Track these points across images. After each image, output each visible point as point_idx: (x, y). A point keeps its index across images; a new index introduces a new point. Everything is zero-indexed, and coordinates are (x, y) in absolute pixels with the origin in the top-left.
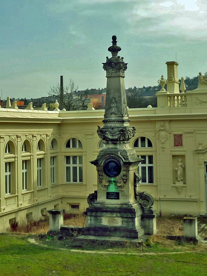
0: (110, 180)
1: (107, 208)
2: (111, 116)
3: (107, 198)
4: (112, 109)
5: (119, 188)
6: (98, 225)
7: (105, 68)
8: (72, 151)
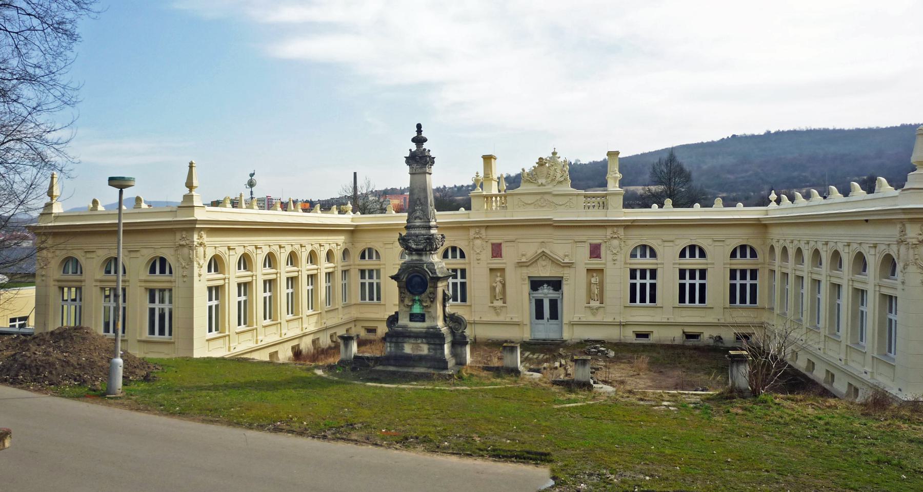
0: (414, 298)
1: (411, 332)
3: (411, 320)
8: (368, 264)
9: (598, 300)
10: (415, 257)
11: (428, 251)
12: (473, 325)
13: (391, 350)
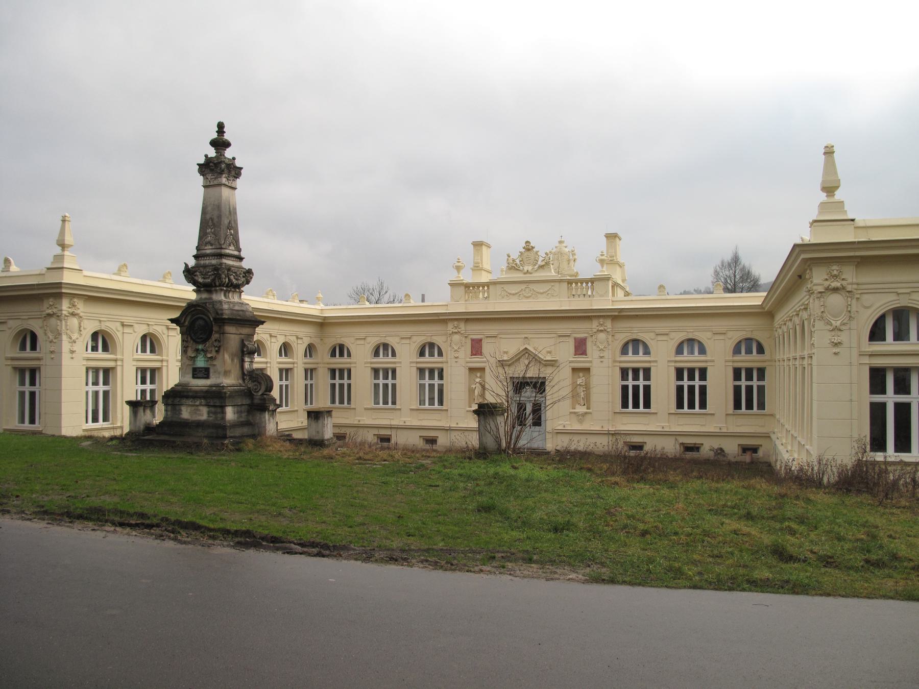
2: (206, 248)
3: (194, 377)
5: (210, 361)
8: (339, 362)
9: (584, 405)
11: (218, 286)
12: (449, 431)
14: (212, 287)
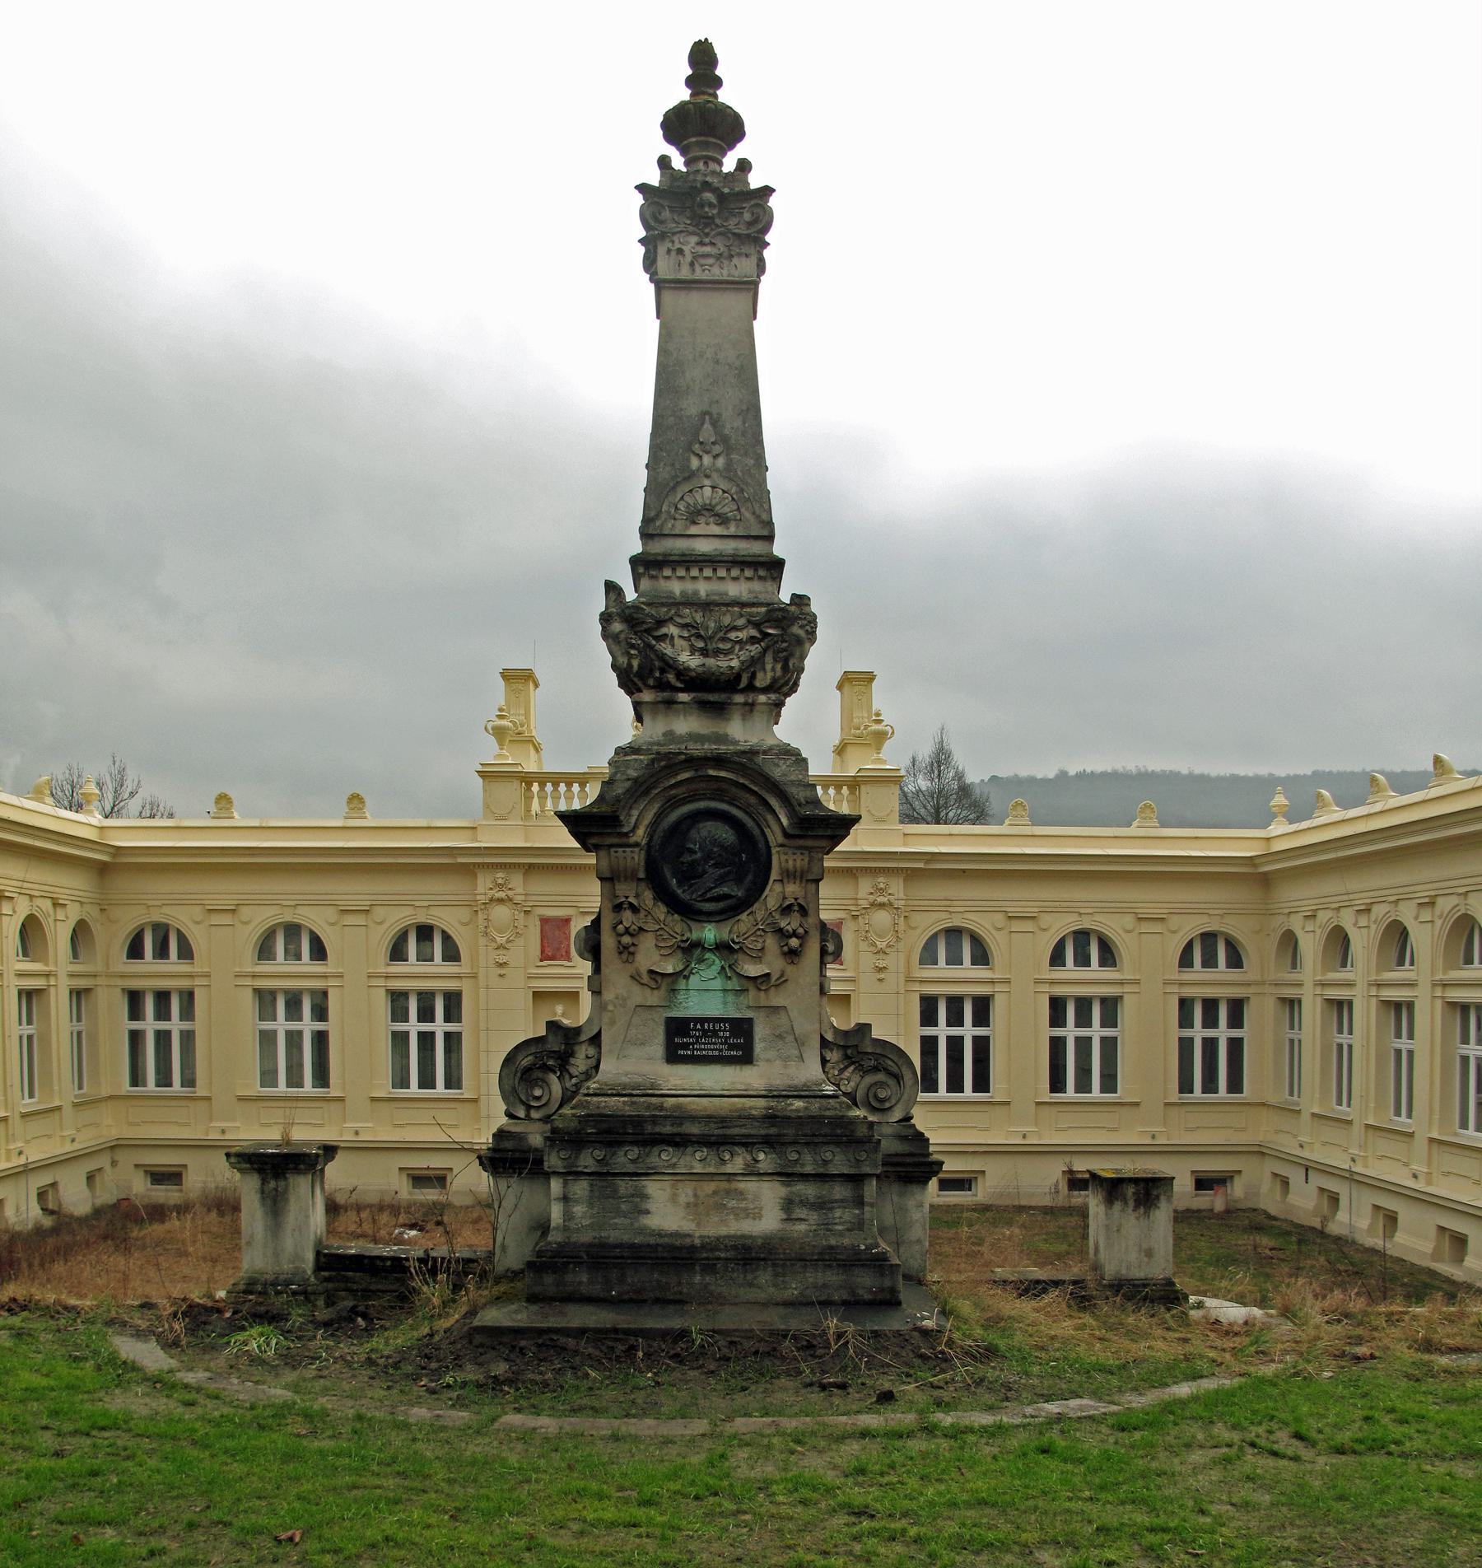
0: (695, 936)
1: (681, 1117)
2: (693, 530)
4: (695, 483)
6: (617, 1232)
7: (656, 220)
8: (151, 972)
10: (687, 725)
13: (568, 1216)
14: (735, 690)
